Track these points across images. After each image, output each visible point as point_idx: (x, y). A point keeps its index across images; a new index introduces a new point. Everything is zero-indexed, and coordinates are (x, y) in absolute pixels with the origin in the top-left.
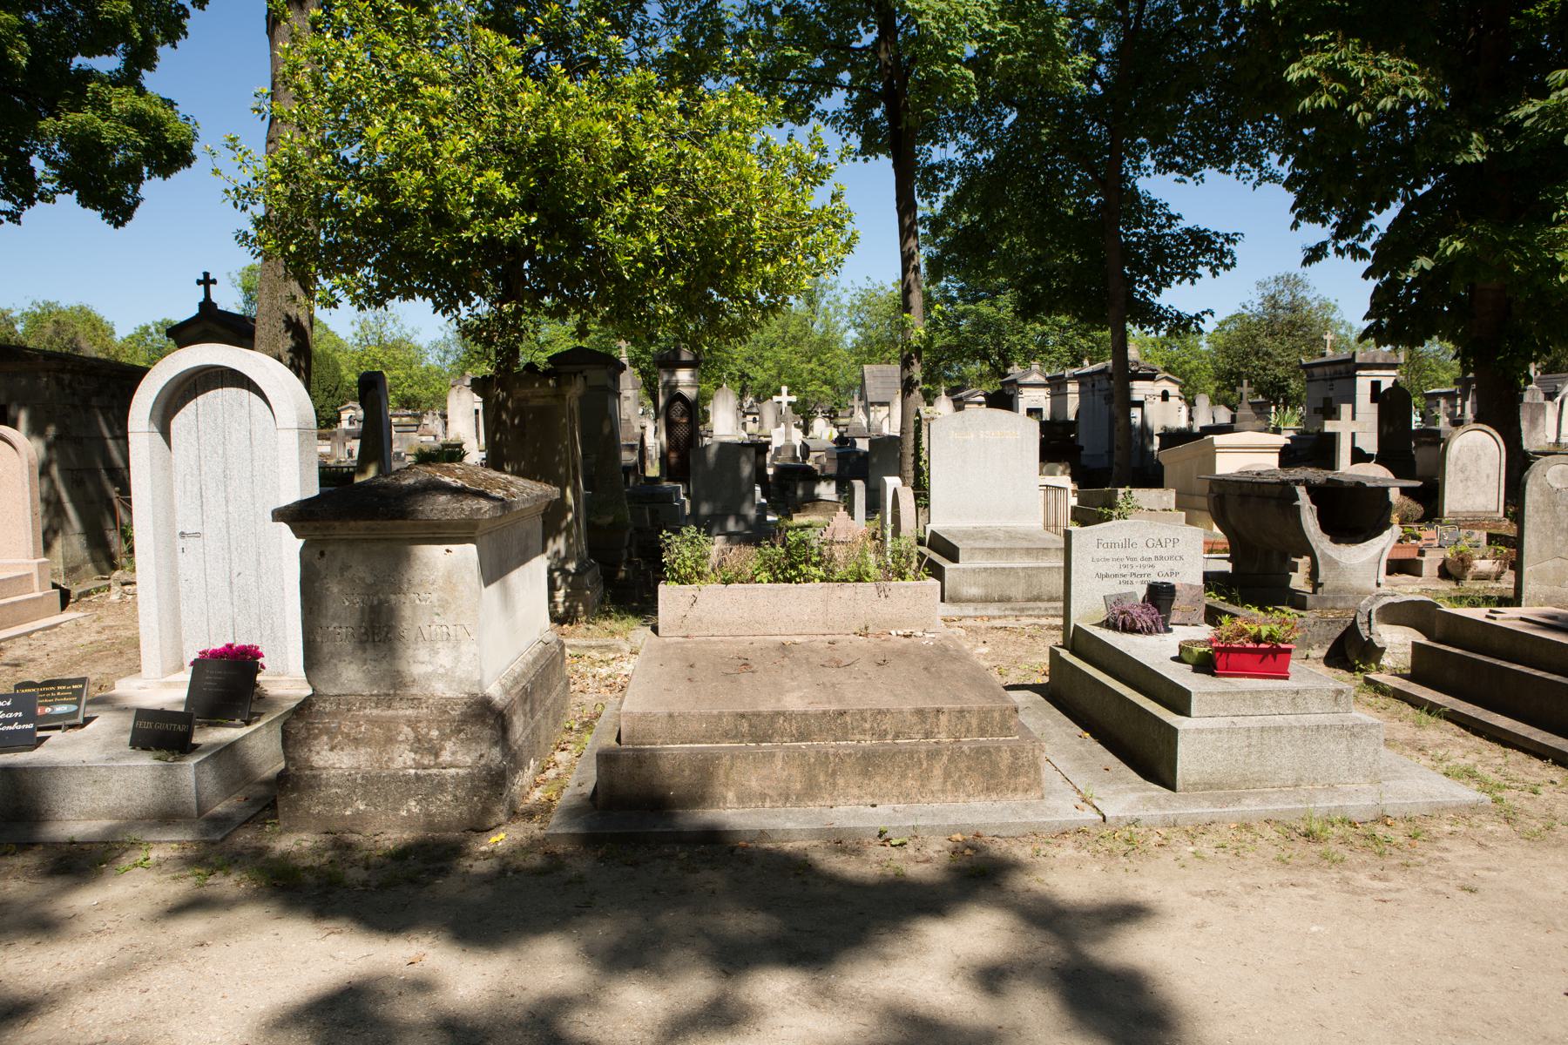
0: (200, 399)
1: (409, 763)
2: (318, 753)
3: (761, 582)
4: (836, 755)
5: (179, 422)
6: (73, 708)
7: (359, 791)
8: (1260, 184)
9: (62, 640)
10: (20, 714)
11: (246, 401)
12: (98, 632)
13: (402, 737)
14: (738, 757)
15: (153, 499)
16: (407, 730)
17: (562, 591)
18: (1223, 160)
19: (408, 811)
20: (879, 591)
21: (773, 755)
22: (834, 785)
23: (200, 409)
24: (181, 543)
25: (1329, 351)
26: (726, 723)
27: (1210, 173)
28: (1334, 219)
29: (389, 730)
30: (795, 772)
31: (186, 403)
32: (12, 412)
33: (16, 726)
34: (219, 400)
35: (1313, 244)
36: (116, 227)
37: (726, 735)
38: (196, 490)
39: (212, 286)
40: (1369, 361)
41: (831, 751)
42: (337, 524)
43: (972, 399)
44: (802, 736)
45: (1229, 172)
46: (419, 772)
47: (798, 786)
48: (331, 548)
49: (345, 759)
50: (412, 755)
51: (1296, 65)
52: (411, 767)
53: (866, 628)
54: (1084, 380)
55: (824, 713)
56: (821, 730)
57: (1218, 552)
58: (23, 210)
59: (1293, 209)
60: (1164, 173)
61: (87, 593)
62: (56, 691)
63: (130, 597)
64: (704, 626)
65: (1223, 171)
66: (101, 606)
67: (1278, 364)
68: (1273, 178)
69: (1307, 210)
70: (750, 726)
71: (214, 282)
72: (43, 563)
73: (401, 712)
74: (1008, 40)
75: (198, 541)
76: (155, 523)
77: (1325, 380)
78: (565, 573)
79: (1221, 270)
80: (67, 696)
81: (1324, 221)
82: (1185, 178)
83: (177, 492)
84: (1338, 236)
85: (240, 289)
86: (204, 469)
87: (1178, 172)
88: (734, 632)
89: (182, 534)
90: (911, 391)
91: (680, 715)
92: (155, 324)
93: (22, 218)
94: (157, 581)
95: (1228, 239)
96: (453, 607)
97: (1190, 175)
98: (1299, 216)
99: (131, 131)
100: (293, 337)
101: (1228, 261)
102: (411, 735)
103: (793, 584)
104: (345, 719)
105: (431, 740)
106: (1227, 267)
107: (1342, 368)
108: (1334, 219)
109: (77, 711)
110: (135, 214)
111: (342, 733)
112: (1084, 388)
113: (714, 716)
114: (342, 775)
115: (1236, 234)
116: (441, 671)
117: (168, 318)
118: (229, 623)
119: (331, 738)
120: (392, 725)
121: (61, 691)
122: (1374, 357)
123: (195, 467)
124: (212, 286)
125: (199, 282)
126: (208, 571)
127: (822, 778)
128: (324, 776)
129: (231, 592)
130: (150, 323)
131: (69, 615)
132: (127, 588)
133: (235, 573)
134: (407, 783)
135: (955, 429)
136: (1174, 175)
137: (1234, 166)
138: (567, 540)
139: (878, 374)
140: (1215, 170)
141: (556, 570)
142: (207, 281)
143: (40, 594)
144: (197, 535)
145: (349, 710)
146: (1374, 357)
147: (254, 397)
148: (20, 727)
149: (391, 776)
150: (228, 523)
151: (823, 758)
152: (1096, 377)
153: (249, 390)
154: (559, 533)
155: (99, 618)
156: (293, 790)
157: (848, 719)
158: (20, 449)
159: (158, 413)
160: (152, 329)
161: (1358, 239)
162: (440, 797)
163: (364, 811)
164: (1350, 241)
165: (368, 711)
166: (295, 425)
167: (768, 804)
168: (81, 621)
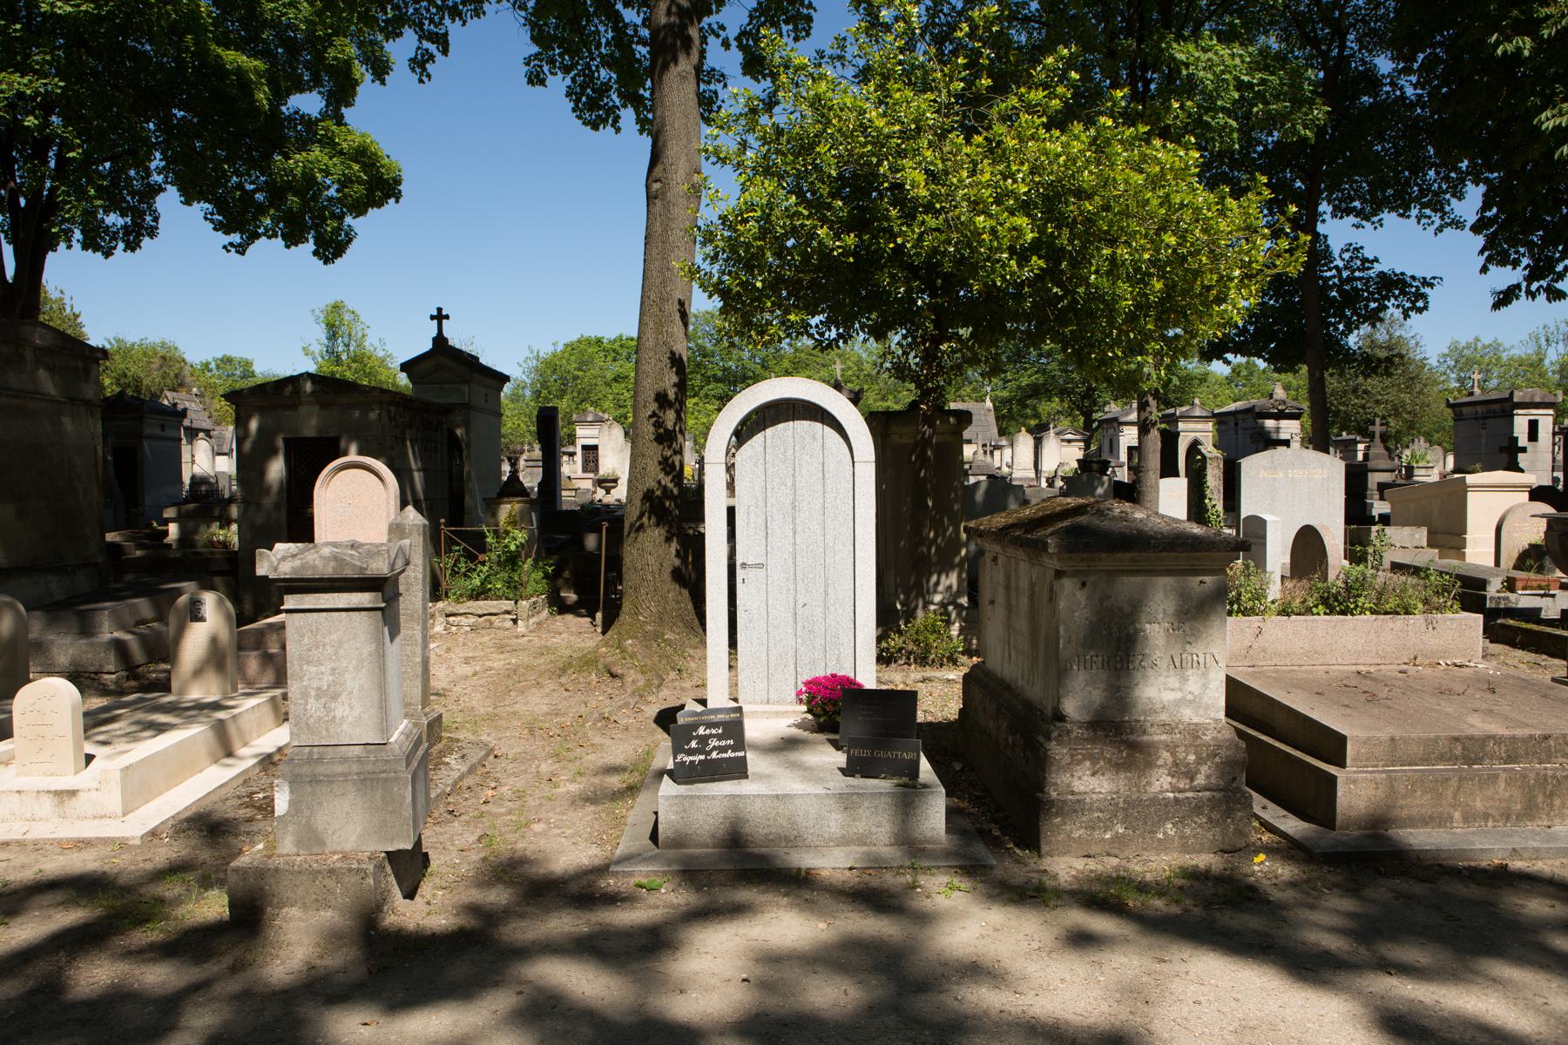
0: (769, 431)
1: (1166, 786)
3: (1318, 614)
4: (1554, 777)
7: (1120, 815)
8: (1441, 231)
10: (732, 742)
13: (1160, 762)
14: (1465, 779)
16: (1166, 755)
17: (957, 625)
18: (1401, 205)
19: (1165, 833)
20: (1428, 623)
21: (1496, 777)
22: (1551, 806)
25: (1476, 390)
26: (1442, 747)
27: (1389, 217)
28: (1525, 261)
30: (1516, 793)
32: (343, 444)
33: (730, 754)
34: (790, 433)
35: (1504, 287)
36: (325, 263)
37: (1442, 758)
38: (761, 521)
39: (444, 321)
40: (1527, 400)
41: (1550, 773)
42: (1104, 555)
45: (1409, 217)
47: (1519, 807)
48: (1092, 579)
49: (1105, 784)
50: (1169, 779)
51: (1548, 113)
53: (1415, 658)
54: (1225, 419)
55: (1531, 737)
56: (1527, 754)
57: (1532, 588)
59: (1481, 252)
60: (1341, 217)
63: (454, 629)
65: (1401, 215)
67: (1378, 402)
68: (1458, 224)
69: (1496, 254)
71: (447, 317)
74: (1265, 90)
75: (762, 573)
77: (1476, 419)
78: (959, 607)
79: (1412, 314)
81: (1516, 264)
82: (1364, 223)
84: (1530, 279)
85: (324, 326)
86: (771, 500)
87: (1356, 216)
90: (1149, 431)
92: (215, 360)
95: (1425, 283)
97: (1368, 220)
98: (1489, 260)
99: (356, 167)
100: (677, 373)
101: (1420, 304)
102: (1170, 760)
103: (1349, 617)
106: (1420, 310)
107: (1497, 407)
108: (1525, 261)
112: (1224, 427)
113: (1431, 740)
114: (1105, 799)
115: (1434, 278)
116: (1190, 697)
117: (181, 348)
118: (791, 653)
119: (1094, 764)
122: (1532, 396)
124: (444, 321)
125: (432, 318)
126: (770, 602)
127: (1540, 799)
130: (210, 360)
132: (451, 619)
133: (800, 603)
134: (1166, 806)
135: (1265, 468)
136: (1352, 219)
137: (1414, 212)
138: (959, 576)
140: (1394, 215)
141: (949, 604)
142: (440, 317)
144: (760, 566)
146: (1532, 396)
148: (733, 755)
149: (1150, 799)
151: (1542, 780)
152: (1240, 417)
154: (952, 568)
156: (1057, 815)
157: (1552, 743)
160: (213, 366)
161: (1552, 280)
162: (1196, 819)
163: (1123, 834)
164: (1544, 283)
167: (1490, 824)
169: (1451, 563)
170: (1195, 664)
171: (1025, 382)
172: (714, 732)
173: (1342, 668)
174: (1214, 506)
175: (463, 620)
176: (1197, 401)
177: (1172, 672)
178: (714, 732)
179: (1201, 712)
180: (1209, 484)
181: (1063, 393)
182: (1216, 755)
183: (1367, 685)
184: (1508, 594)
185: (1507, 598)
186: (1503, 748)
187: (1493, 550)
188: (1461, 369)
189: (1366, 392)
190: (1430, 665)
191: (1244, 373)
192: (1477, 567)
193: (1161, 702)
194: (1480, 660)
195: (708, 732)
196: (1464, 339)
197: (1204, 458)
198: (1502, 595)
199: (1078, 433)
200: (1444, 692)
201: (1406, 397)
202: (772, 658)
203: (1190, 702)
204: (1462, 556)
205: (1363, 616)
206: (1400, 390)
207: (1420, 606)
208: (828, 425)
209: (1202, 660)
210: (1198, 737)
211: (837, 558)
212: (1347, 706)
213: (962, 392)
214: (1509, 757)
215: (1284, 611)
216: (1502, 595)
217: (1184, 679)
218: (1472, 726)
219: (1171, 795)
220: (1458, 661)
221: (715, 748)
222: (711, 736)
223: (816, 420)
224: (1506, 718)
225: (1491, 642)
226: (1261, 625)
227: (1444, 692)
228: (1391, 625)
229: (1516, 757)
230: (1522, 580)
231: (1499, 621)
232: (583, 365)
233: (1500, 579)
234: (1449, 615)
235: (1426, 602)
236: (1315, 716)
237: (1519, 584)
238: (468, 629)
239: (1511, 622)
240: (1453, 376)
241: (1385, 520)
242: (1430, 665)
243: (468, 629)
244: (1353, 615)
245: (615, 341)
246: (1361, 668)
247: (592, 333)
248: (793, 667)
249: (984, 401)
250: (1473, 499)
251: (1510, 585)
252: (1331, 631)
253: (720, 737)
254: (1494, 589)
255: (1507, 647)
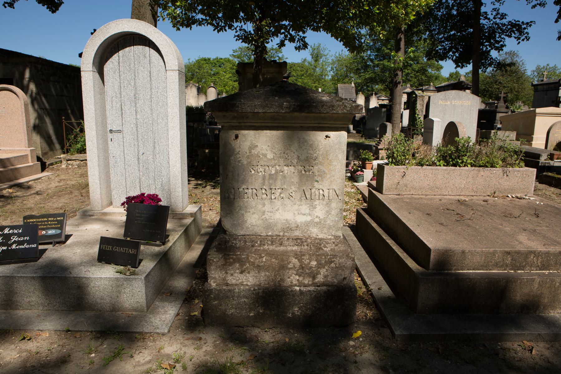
0: (121, 53)
2: (232, 275)
3: (440, 165)
5: (109, 67)
6: (59, 231)
9: (43, 185)
11: (148, 54)
12: (59, 182)
13: (290, 266)
15: (95, 110)
20: (504, 173)
23: (121, 59)
24: (110, 136)
29: (282, 260)
31: (112, 56)
33: (26, 246)
34: (132, 54)
37: (496, 265)
38: (118, 106)
43: (380, 98)
44: (544, 267)
46: (302, 288)
50: (297, 277)
52: (296, 285)
53: (495, 193)
56: (556, 264)
58: (15, 2)
61: (52, 164)
62: (48, 221)
63: (70, 166)
64: (408, 189)
66: (58, 170)
67: (504, 87)
70: (512, 260)
72: (33, 150)
73: (289, 248)
75: (120, 135)
76: (96, 124)
77: (544, 91)
80: (55, 224)
83: (108, 107)
86: (123, 94)
88: (424, 193)
89: (111, 131)
91: (469, 251)
93: (15, 6)
94: (98, 157)
96: (328, 176)
102: (298, 264)
103: (458, 168)
104: (251, 253)
105: (311, 267)
107: (552, 86)
109: (61, 234)
110: (60, 8)
111: (249, 262)
113: (490, 253)
115: (531, 22)
116: (317, 220)
118: (138, 181)
119: (242, 265)
120: (284, 258)
121: (51, 221)
123: (118, 93)
128: (237, 290)
129: (139, 163)
131: (45, 174)
132: (69, 162)
133: (141, 153)
135: (441, 100)
139: (343, 88)
143: (32, 164)
144: (119, 131)
145: (253, 246)
147: (153, 51)
150: (137, 125)
153: (150, 47)
155: (58, 175)
158: (20, 96)
159: (97, 61)
165: (266, 247)
166: (177, 68)
168: (51, 176)
169: (525, 148)
170: (321, 197)
171: (367, 76)
172: (16, 231)
173: (453, 197)
174: (419, 118)
175: (74, 163)
176: (432, 84)
177: (304, 202)
178: (16, 231)
179: (325, 230)
180: (418, 108)
181: (383, 81)
182: (331, 262)
183: (461, 209)
184: (550, 161)
185: (549, 163)
186: (540, 260)
187: (545, 142)
188: (540, 77)
189: (500, 83)
190: (503, 197)
191: (454, 76)
192: (536, 149)
193: (296, 223)
194: (532, 195)
195: (11, 231)
196: (543, 64)
197: (416, 96)
198: (547, 161)
199: (386, 97)
200: (507, 215)
201: (516, 85)
202: (128, 183)
203: (317, 223)
204: (531, 145)
205: (466, 168)
206: (514, 82)
207: (500, 162)
208: (152, 48)
209: (326, 194)
210: (321, 248)
211: (159, 127)
212: (442, 224)
213: (345, 81)
214: (543, 265)
215: (420, 163)
216: (547, 161)
217: (313, 207)
218: (521, 243)
219: (298, 288)
220: (519, 195)
221: (15, 242)
222: (14, 234)
223: (146, 46)
224: (544, 237)
225: (540, 183)
226: (405, 171)
227: (507, 215)
228: (482, 173)
229: (548, 266)
230: (557, 155)
231: (544, 174)
232: (200, 67)
233: (546, 154)
234: (517, 168)
235: (504, 160)
236: (417, 231)
237: (555, 157)
238: (76, 166)
239: (550, 174)
240: (536, 79)
241: (499, 129)
242: (503, 197)
243: (76, 166)
244: (460, 166)
245: (215, 59)
246: (463, 198)
247: (206, 56)
248: (139, 188)
249: (351, 84)
250: (538, 120)
251: (551, 157)
252: (446, 176)
253: (19, 235)
254: (543, 159)
255: (547, 186)
